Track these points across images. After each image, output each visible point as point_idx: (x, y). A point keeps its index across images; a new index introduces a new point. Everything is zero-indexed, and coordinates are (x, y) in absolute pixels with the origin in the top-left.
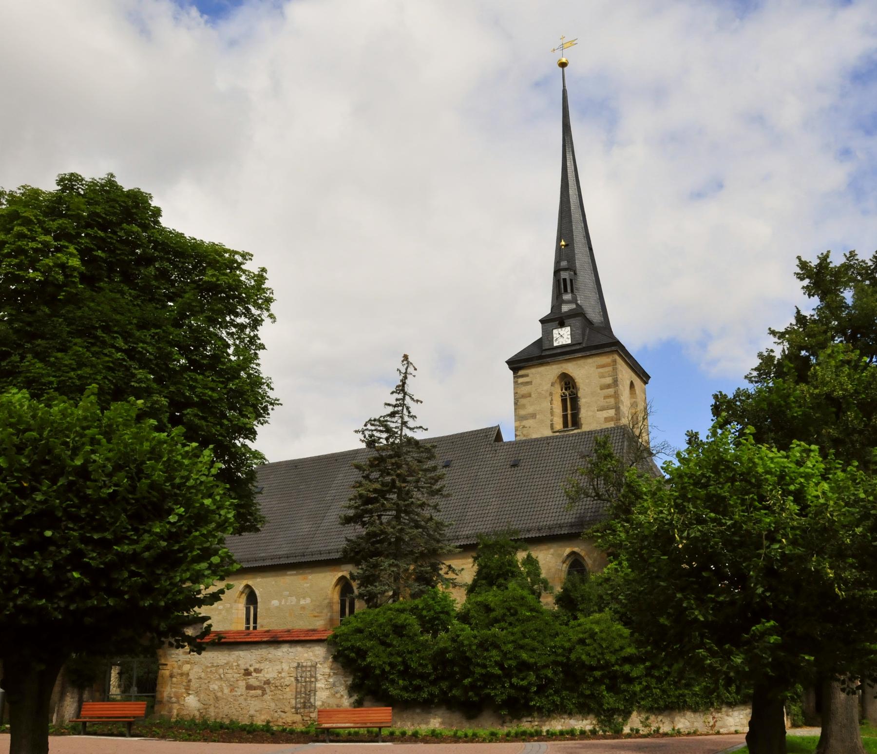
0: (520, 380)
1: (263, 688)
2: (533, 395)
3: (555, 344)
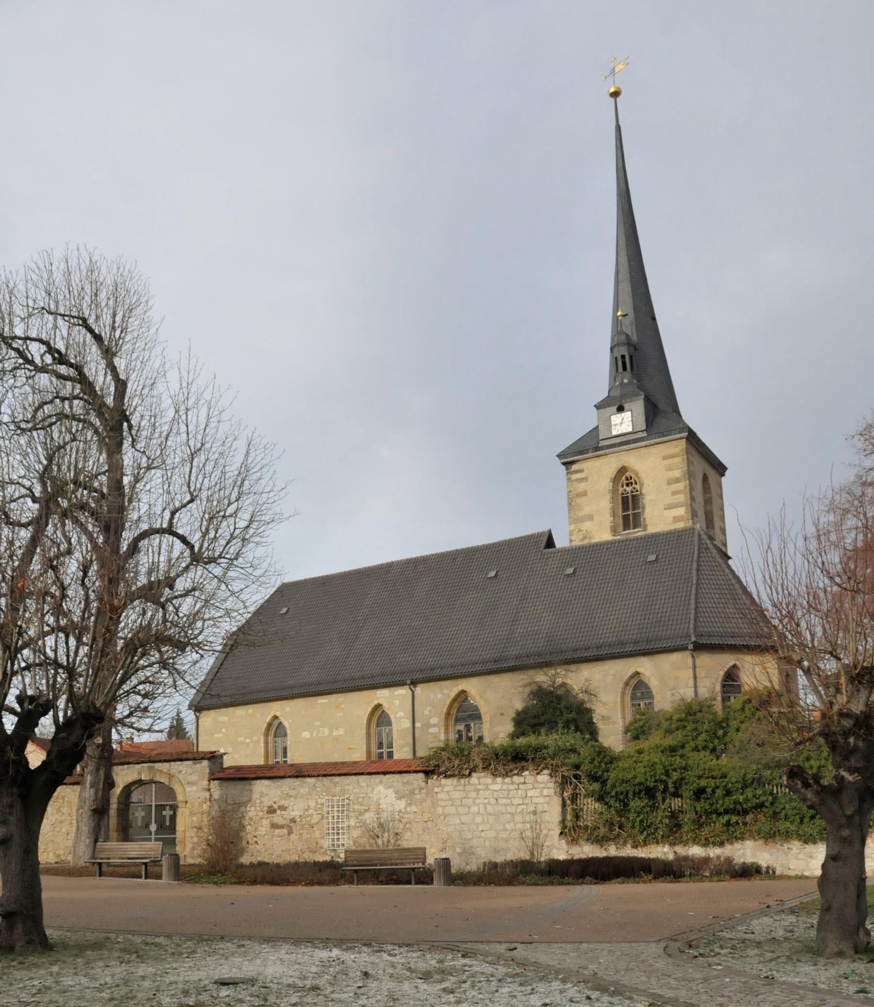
0: (574, 477)
1: (288, 826)
2: (589, 494)
3: (614, 433)
